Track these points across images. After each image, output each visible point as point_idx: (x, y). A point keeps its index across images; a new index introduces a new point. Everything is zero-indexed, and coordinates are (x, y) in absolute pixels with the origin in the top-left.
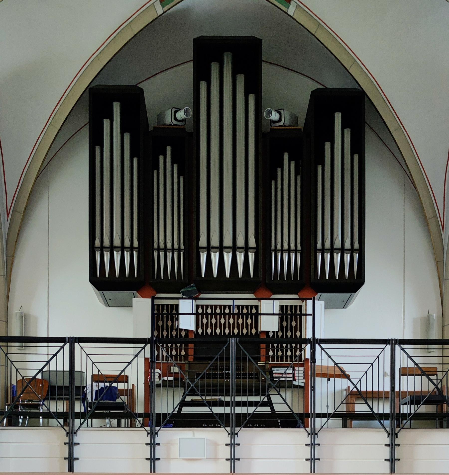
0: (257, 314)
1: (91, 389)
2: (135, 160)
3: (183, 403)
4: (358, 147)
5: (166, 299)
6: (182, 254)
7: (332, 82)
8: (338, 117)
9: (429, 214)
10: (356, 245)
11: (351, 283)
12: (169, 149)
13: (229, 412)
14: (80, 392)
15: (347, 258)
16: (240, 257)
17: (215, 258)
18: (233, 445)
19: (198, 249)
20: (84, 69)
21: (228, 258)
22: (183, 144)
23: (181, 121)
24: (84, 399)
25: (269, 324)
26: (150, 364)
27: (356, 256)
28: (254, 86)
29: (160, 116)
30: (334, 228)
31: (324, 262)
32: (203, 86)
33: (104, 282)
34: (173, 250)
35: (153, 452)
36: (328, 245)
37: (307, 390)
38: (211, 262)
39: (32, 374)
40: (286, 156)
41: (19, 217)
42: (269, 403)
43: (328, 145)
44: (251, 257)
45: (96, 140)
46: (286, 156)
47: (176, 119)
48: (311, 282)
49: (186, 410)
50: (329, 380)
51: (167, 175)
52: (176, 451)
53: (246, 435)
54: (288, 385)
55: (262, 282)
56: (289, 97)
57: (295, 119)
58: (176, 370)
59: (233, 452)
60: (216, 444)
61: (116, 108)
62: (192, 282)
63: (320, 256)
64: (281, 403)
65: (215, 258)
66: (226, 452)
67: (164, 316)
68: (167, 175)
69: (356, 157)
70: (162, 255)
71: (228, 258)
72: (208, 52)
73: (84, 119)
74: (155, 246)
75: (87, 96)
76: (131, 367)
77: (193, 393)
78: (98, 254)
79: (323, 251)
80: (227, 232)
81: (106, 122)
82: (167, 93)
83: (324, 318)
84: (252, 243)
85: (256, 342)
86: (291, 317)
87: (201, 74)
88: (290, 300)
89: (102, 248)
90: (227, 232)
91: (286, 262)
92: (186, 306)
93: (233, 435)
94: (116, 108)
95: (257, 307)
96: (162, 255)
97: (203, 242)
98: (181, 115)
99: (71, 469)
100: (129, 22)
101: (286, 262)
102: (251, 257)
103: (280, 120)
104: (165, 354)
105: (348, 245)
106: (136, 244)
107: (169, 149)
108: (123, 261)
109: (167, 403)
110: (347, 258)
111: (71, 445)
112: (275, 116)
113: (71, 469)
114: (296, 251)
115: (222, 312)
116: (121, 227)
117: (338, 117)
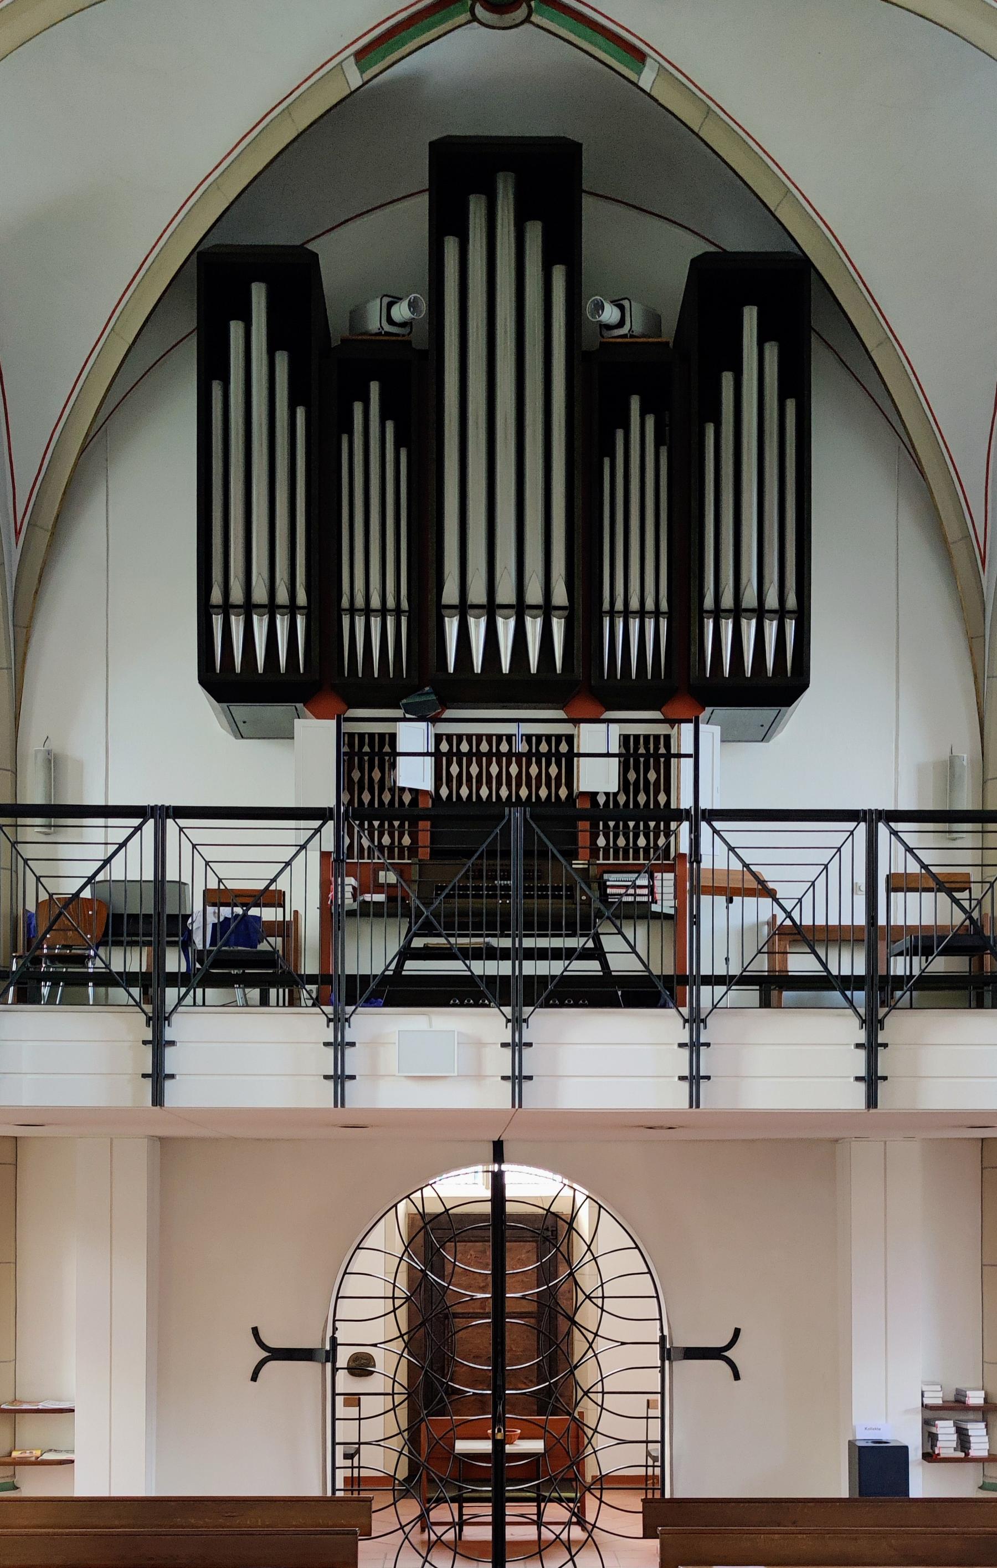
0: (572, 756)
1: (203, 922)
2: (300, 412)
3: (407, 953)
4: (795, 384)
5: (368, 720)
6: (404, 620)
7: (738, 238)
8: (750, 316)
9: (953, 532)
10: (791, 602)
11: (778, 686)
12: (374, 387)
13: (508, 972)
14: (177, 929)
15: (771, 629)
16: (534, 628)
17: (477, 629)
18: (517, 1046)
19: (441, 610)
20: (187, 209)
21: (506, 629)
22: (407, 377)
23: (403, 325)
24: (186, 943)
25: (598, 777)
26: (334, 865)
27: (791, 626)
28: (564, 248)
29: (356, 315)
30: (741, 564)
31: (719, 639)
32: (451, 246)
33: (230, 683)
34: (383, 612)
35: (339, 1060)
36: (727, 601)
37: (681, 924)
38: (469, 638)
39: (70, 887)
40: (635, 404)
41: (42, 538)
42: (598, 953)
43: (727, 379)
44: (558, 627)
45: (213, 367)
46: (635, 404)
47: (390, 321)
48: (690, 684)
49: (413, 967)
50: (730, 901)
51: (371, 442)
52: (390, 1059)
53: (546, 1023)
54: (640, 912)
55: (583, 683)
56: (641, 271)
57: (654, 320)
58: (392, 878)
59: (517, 1062)
60: (479, 1044)
61: (258, 295)
62: (428, 682)
63: (607, 622)
64: (624, 953)
65: (477, 629)
66: (502, 1062)
67: (364, 760)
68: (371, 442)
69: (791, 405)
70: (360, 622)
71: (506, 629)
72: (462, 171)
73: (186, 320)
74: (345, 603)
75: (193, 269)
76: (291, 873)
77: (427, 929)
78: (217, 621)
79: (718, 613)
80: (504, 572)
81: (236, 329)
82: (371, 264)
83: (719, 763)
84: (560, 596)
85: (568, 817)
86: (646, 762)
87: (447, 221)
88: (643, 723)
89: (227, 608)
90: (504, 572)
91: (636, 639)
92: (413, 736)
93: (517, 1022)
94: (258, 295)
95: (570, 739)
96: (360, 622)
97: (450, 594)
98: (401, 312)
99: (158, 1099)
100: (287, 105)
101: (636, 639)
102: (558, 627)
103: (621, 324)
104: (366, 843)
105: (772, 601)
106: (302, 599)
107: (374, 387)
108: (273, 638)
109: (371, 952)
110: (771, 629)
111: (159, 1045)
112: (610, 314)
113: (158, 1099)
114: (657, 614)
115: (493, 751)
116: (269, 560)
117: (750, 316)
